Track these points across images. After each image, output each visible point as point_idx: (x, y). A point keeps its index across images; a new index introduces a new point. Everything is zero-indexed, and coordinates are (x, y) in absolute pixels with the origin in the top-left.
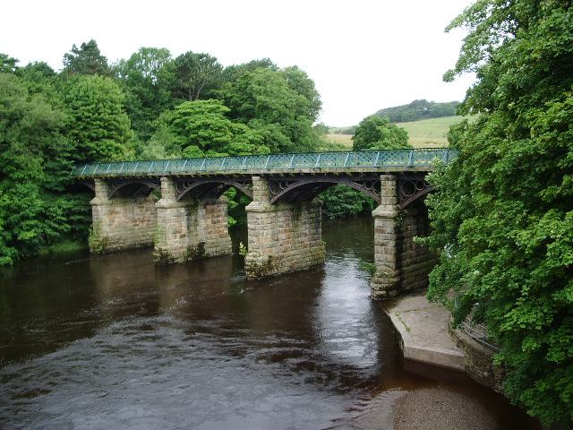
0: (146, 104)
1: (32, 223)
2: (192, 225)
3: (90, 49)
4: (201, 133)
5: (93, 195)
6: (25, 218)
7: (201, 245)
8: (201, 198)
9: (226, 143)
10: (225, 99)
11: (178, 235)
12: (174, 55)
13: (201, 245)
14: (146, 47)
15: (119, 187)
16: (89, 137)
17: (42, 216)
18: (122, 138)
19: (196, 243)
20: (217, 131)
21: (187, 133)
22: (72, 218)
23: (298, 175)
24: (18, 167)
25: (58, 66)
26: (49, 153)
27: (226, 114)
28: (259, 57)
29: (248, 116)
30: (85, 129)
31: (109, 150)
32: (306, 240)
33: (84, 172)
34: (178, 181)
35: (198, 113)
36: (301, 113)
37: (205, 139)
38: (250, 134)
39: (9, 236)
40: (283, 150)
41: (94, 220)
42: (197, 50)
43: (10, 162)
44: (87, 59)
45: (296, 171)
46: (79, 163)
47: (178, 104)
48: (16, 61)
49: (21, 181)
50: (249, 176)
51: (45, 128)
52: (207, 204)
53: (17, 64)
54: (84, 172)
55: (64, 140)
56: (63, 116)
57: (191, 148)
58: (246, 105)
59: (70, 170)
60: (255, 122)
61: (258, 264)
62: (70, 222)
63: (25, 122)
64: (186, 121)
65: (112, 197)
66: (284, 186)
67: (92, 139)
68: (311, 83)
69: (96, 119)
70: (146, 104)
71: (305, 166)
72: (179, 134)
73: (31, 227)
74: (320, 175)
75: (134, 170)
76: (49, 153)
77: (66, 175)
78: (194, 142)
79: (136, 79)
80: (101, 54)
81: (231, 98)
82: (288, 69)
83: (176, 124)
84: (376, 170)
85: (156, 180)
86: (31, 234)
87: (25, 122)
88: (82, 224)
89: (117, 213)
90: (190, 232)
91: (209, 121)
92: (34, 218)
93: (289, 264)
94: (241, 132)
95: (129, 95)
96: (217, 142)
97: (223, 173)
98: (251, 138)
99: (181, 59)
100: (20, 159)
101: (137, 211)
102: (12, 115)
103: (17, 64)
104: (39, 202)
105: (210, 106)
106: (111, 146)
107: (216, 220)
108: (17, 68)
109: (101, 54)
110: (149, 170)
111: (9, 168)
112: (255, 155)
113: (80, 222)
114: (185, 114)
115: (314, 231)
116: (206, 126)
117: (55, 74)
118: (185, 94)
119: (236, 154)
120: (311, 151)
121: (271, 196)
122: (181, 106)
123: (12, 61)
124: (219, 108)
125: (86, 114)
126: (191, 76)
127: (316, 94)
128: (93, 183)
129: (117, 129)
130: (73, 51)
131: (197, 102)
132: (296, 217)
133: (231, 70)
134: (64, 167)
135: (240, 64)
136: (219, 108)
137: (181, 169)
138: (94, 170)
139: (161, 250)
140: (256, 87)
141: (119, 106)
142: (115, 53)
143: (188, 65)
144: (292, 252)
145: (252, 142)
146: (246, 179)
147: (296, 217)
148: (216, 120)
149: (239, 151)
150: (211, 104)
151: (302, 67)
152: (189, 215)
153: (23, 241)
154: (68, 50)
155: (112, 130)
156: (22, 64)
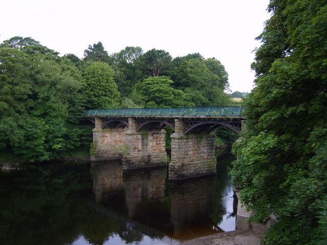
0: (128, 78)
1: (60, 140)
2: (144, 145)
3: (99, 47)
4: (156, 94)
5: (94, 126)
6: (56, 137)
7: (149, 156)
8: (150, 130)
9: (170, 100)
10: (173, 76)
11: (136, 150)
12: (145, 51)
13: (149, 156)
14: (129, 46)
15: (108, 122)
16: (94, 95)
17: (66, 137)
18: (113, 96)
19: (146, 154)
20: (166, 93)
21: (149, 94)
22: (82, 138)
23: (198, 119)
24: (54, 110)
25: (81, 56)
26: (71, 102)
27: (171, 85)
28: (192, 52)
29: (186, 85)
30: (92, 90)
31: (105, 102)
32: (205, 156)
33: (90, 113)
34: (138, 120)
35: (155, 83)
36: (215, 84)
37: (158, 97)
38: (184, 95)
39: (47, 146)
40: (204, 105)
41: (94, 140)
42: (158, 48)
43: (50, 107)
44: (97, 52)
45: (197, 117)
46: (87, 108)
47: (146, 78)
48: (58, 53)
49: (56, 117)
50: (173, 119)
51: (69, 89)
52: (154, 134)
53: (59, 55)
54: (90, 113)
55: (80, 96)
56: (79, 84)
57: (150, 103)
58: (184, 80)
59: (83, 112)
60: (188, 89)
61: (176, 167)
62: (81, 141)
63: (58, 86)
64: (149, 88)
65: (104, 128)
66: (191, 124)
67: (96, 96)
68: (222, 68)
69: (98, 85)
70: (128, 78)
71: (216, 113)
72: (145, 95)
73: (60, 142)
74: (209, 119)
75: (115, 114)
76: (71, 102)
77: (80, 115)
78: (153, 99)
79: (124, 63)
80: (104, 50)
81: (177, 75)
82: (209, 59)
83: (144, 89)
84: (239, 117)
85: (126, 119)
86: (59, 146)
87: (58, 86)
88: (86, 142)
89: (106, 137)
90: (143, 148)
91: (161, 88)
92: (62, 137)
93: (194, 168)
94: (179, 94)
95: (118, 72)
96: (165, 100)
97: (160, 117)
98: (185, 98)
99: (148, 53)
100: (55, 106)
101: (118, 136)
102: (53, 82)
103: (59, 55)
104: (64, 129)
105: (162, 80)
106: (106, 100)
107: (158, 142)
108: (58, 57)
109: (104, 50)
110: (123, 113)
111: (50, 110)
112: (186, 107)
113: (87, 140)
114: (149, 84)
115: (209, 151)
116: (160, 91)
117: (224, 102)
118: (151, 73)
119: (175, 106)
120: (220, 106)
121: (184, 130)
122: (147, 79)
123: (57, 53)
124: (167, 81)
125: (93, 82)
126: (154, 62)
127: (226, 73)
128: (94, 119)
129: (110, 91)
130: (89, 48)
131: (157, 77)
132: (198, 143)
133: (178, 59)
134: (80, 111)
135: (182, 56)
136: (167, 81)
137: (138, 114)
138: (96, 113)
139: (126, 158)
140: (189, 69)
141: (111, 78)
142: (112, 49)
143: (153, 56)
144: (196, 162)
145: (185, 100)
146: (171, 120)
147: (198, 143)
148: (165, 87)
149: (177, 105)
150: (163, 78)
151: (218, 58)
152: (143, 139)
153: (55, 149)
154: (87, 48)
155: (107, 91)
156: (61, 55)
